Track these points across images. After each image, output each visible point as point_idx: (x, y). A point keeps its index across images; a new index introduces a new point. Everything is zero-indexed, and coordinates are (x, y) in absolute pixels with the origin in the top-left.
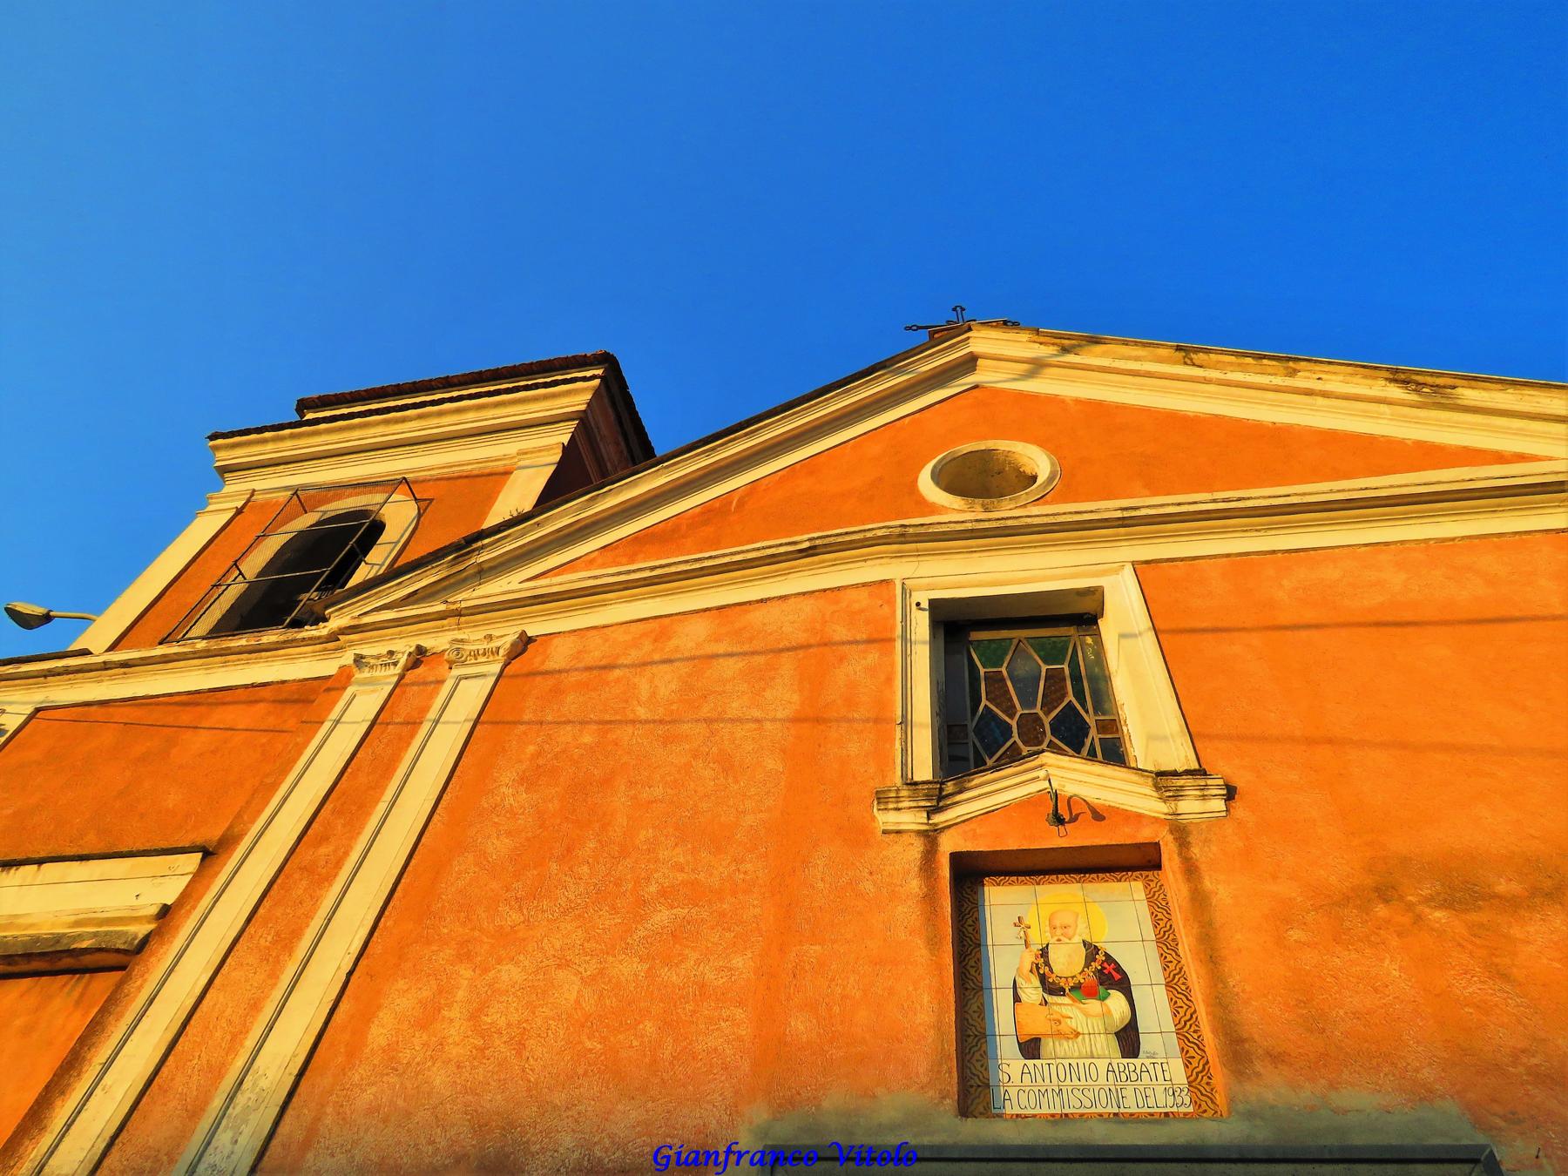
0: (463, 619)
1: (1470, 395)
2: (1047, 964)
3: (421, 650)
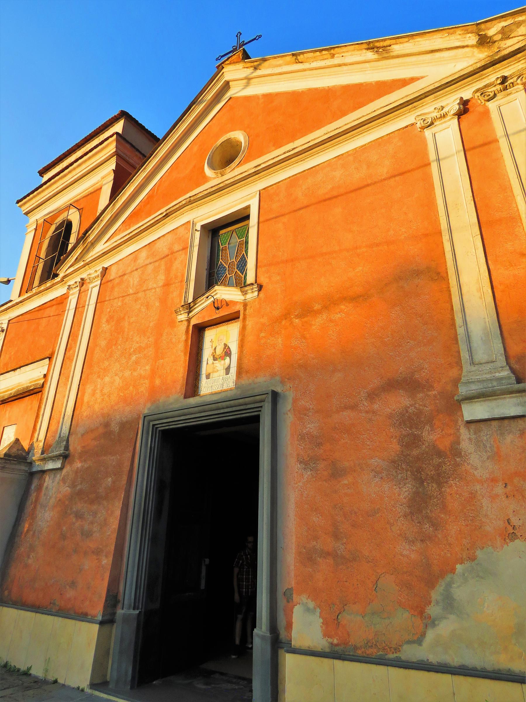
0: (89, 265)
1: (397, 48)
2: (215, 352)
3: (82, 279)
